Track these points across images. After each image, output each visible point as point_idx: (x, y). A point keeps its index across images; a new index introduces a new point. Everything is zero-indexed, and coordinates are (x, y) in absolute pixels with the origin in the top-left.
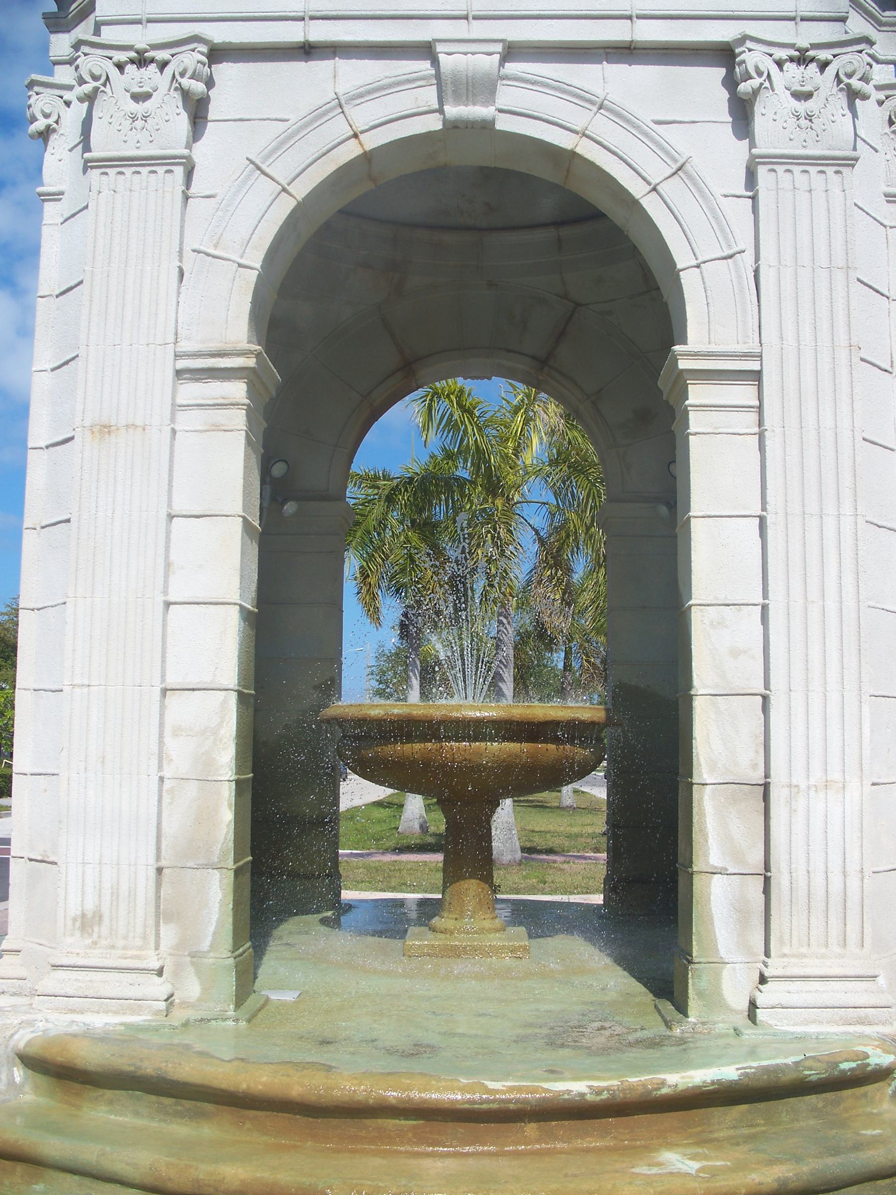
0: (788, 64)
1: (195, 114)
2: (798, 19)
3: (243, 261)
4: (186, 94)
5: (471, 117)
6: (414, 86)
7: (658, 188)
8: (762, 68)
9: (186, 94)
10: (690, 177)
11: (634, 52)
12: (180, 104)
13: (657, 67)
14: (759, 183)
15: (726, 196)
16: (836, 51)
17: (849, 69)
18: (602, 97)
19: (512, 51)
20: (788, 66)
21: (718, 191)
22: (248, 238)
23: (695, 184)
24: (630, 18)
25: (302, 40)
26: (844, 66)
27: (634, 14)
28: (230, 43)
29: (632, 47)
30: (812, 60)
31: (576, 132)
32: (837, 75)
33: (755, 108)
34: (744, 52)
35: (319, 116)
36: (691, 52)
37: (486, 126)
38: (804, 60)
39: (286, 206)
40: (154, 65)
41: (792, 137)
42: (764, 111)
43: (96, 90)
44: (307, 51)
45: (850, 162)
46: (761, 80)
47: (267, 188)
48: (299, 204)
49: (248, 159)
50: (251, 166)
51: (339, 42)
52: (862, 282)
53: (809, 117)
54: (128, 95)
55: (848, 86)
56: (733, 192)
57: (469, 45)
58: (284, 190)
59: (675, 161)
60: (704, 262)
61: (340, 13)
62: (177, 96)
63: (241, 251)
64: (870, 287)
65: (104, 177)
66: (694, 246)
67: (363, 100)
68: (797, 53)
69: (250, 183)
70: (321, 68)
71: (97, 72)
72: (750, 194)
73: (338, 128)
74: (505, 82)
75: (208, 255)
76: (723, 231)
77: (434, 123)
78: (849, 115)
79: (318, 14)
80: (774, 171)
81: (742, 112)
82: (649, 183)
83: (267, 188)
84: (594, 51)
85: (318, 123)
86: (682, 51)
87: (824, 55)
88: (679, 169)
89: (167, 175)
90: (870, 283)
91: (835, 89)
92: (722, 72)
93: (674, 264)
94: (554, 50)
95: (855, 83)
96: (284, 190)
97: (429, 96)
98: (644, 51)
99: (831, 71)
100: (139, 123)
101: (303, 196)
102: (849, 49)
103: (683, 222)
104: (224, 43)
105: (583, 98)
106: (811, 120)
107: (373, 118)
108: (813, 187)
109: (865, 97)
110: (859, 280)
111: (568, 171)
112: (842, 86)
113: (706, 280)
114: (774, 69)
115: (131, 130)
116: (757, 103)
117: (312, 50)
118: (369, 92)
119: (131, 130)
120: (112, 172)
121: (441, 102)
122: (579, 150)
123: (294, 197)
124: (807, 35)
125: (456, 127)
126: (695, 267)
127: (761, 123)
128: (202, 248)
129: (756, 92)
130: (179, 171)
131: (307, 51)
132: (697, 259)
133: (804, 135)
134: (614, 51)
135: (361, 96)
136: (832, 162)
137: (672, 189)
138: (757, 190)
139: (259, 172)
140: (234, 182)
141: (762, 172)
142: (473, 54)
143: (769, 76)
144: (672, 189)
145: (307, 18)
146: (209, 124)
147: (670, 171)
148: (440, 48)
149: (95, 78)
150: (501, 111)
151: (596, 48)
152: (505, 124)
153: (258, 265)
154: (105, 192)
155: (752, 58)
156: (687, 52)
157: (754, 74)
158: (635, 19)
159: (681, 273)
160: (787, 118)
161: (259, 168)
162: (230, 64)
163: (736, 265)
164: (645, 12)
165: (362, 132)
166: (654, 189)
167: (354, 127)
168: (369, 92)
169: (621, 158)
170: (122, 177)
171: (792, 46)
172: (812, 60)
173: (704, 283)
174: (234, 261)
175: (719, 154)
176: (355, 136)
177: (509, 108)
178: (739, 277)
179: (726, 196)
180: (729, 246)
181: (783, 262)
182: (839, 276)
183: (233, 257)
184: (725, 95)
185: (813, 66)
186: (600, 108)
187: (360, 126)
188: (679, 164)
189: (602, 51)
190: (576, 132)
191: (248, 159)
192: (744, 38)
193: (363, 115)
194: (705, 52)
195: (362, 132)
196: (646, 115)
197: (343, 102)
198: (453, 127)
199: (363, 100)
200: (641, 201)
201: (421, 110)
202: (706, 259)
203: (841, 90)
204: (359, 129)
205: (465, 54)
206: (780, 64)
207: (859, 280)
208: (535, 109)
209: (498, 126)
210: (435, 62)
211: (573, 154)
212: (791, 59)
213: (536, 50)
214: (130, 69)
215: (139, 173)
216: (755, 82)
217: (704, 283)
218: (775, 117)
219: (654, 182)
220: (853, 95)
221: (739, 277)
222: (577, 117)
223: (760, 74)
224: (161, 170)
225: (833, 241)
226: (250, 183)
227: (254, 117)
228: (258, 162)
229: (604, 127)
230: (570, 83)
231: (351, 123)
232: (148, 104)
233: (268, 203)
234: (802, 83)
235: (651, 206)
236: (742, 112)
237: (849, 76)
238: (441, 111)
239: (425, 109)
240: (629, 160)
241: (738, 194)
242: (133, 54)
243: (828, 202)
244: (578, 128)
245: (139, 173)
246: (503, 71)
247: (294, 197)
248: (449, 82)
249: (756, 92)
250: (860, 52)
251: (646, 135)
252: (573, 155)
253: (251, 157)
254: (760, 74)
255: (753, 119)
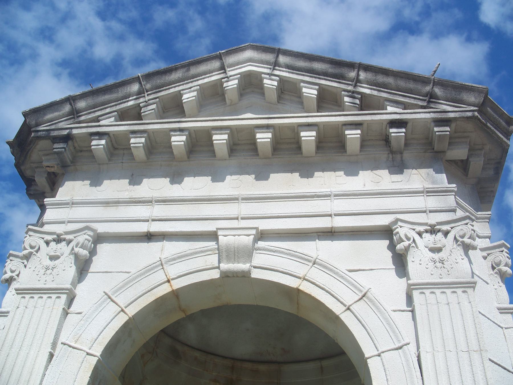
0: (425, 234)
1: (83, 268)
2: (428, 212)
3: (90, 352)
4: (77, 256)
5: (235, 269)
6: (205, 254)
7: (351, 308)
8: (409, 236)
9: (77, 256)
10: (370, 300)
11: (334, 234)
12: (73, 262)
13: (348, 242)
14: (415, 301)
15: (395, 311)
16: (453, 225)
17: (461, 233)
18: (315, 257)
19: (262, 235)
20: (424, 235)
21: (389, 309)
22: (95, 338)
23: (374, 304)
24: (330, 215)
25: (146, 231)
26: (458, 232)
27: (333, 213)
28: (108, 233)
29: (333, 231)
30: (439, 231)
31: (299, 278)
32: (455, 238)
33: (408, 258)
34: (398, 228)
35: (149, 270)
36: (367, 233)
37: (245, 275)
38: (434, 232)
39: (123, 319)
40: (64, 242)
41: (432, 273)
42: (413, 260)
43: (31, 254)
44: (149, 237)
45: (472, 285)
46: (410, 242)
47: (114, 309)
48: (130, 318)
49: (104, 292)
50: (106, 296)
51: (166, 232)
52: (493, 361)
53: (442, 261)
54: (48, 257)
55: (463, 242)
56: (399, 309)
57: (236, 231)
58: (122, 310)
59: (361, 291)
60: (383, 352)
61: (168, 217)
62: (73, 257)
63: (90, 345)
64: (499, 365)
65: (23, 300)
66: (376, 342)
67: (175, 262)
68: (429, 228)
69: (103, 306)
70: (155, 246)
71: (33, 244)
72: (410, 309)
73: (160, 277)
74: (258, 252)
75: (70, 346)
76: (394, 332)
77: (215, 275)
78: (466, 259)
79: (157, 218)
80: (423, 293)
81: (400, 262)
82: (345, 306)
83: (114, 309)
84: (311, 234)
85: (148, 274)
86: (362, 233)
87: (445, 228)
88: (364, 296)
89: (57, 299)
90: (498, 362)
91: (455, 246)
92: (387, 242)
93: (362, 354)
94: (288, 235)
95: (466, 240)
96: (122, 310)
97: (214, 260)
98: (340, 233)
99: (451, 236)
100: (49, 272)
101: (133, 314)
102: (460, 223)
103: (367, 328)
104: (105, 233)
105: (304, 259)
106: (443, 263)
107: (180, 271)
108: (450, 301)
109: (474, 248)
110: (490, 360)
111: (298, 304)
112: (459, 243)
113: (385, 363)
114: (417, 237)
115: (44, 274)
116: (409, 256)
117: (152, 237)
118: (179, 257)
119: (44, 274)
120: (27, 296)
121: (219, 262)
122: (301, 288)
123: (128, 315)
124: (434, 219)
125: (228, 276)
126: (377, 356)
127: (412, 267)
128: (67, 342)
129: (407, 249)
130: (64, 297)
131: (149, 237)
132: (378, 351)
133: (440, 272)
134: (323, 234)
135: (174, 259)
136: (459, 285)
137: (359, 308)
138: (414, 305)
139: (110, 300)
140: (94, 305)
141: (416, 294)
142: (239, 235)
143: (414, 240)
144: (359, 308)
145: (150, 220)
146: (89, 274)
147: (358, 298)
148: (220, 233)
149: (32, 247)
150: (255, 267)
151: (312, 233)
152: (256, 274)
153: (98, 354)
154: (22, 308)
155: (402, 231)
156: (365, 233)
157: (404, 239)
158: (333, 216)
159: (368, 360)
160: (428, 262)
161: (110, 298)
162: (107, 244)
163: (405, 353)
164: (339, 212)
165: (173, 279)
166: (348, 309)
167: (168, 276)
168: (179, 257)
169: (327, 292)
170: (32, 300)
171: (426, 224)
172: (439, 231)
173: (384, 366)
174: (84, 351)
175: (389, 287)
176: (168, 281)
177: (260, 265)
178: (407, 361)
179: (395, 311)
180: (399, 341)
181: (436, 349)
182: (476, 356)
183: (84, 349)
184: (390, 254)
185: (440, 235)
186: (314, 264)
187: (172, 276)
188: (363, 293)
189: (315, 234)
190: (299, 278)
191: (104, 292)
192: (397, 220)
193: (173, 271)
194: (376, 232)
195: (173, 279)
196: (342, 267)
197: (163, 263)
198: (226, 275)
199: (175, 262)
200: (340, 316)
201: (208, 267)
202: (384, 350)
203: (459, 245)
204: (171, 278)
205: (234, 236)
206: (420, 234)
207: (490, 360)
208: (276, 266)
209: (253, 276)
210: (218, 243)
211: (298, 291)
212: (426, 231)
213: (276, 235)
214: (53, 244)
215: (42, 297)
216: (406, 243)
217: (384, 366)
218: (420, 263)
219: (348, 305)
220: (467, 248)
221: (407, 361)
222: (300, 269)
223: (408, 239)
224: (54, 296)
225: (468, 333)
226: (103, 306)
227: (113, 271)
228: (110, 294)
229: (316, 274)
230: (295, 251)
231: (167, 274)
232: (57, 262)
233: (111, 318)
234: (435, 243)
235: (347, 319)
236: (400, 262)
237: (462, 237)
238: (218, 268)
239: (211, 266)
240: (332, 292)
241: (402, 309)
242: (55, 236)
243: (461, 310)
244: (301, 276)
245: (42, 297)
246: (256, 246)
247: (128, 315)
248: (224, 250)
249: (407, 249)
250: (467, 224)
251: (342, 277)
252: (298, 291)
253: (106, 291)
254: (408, 239)
255: (407, 265)
